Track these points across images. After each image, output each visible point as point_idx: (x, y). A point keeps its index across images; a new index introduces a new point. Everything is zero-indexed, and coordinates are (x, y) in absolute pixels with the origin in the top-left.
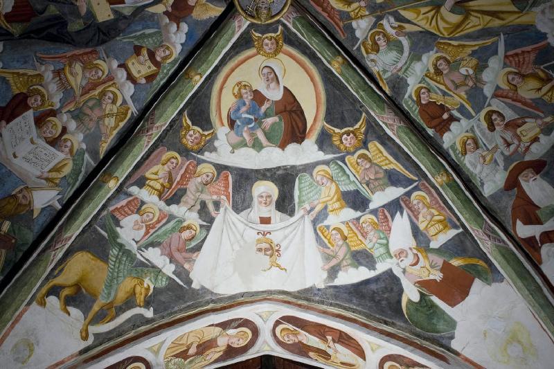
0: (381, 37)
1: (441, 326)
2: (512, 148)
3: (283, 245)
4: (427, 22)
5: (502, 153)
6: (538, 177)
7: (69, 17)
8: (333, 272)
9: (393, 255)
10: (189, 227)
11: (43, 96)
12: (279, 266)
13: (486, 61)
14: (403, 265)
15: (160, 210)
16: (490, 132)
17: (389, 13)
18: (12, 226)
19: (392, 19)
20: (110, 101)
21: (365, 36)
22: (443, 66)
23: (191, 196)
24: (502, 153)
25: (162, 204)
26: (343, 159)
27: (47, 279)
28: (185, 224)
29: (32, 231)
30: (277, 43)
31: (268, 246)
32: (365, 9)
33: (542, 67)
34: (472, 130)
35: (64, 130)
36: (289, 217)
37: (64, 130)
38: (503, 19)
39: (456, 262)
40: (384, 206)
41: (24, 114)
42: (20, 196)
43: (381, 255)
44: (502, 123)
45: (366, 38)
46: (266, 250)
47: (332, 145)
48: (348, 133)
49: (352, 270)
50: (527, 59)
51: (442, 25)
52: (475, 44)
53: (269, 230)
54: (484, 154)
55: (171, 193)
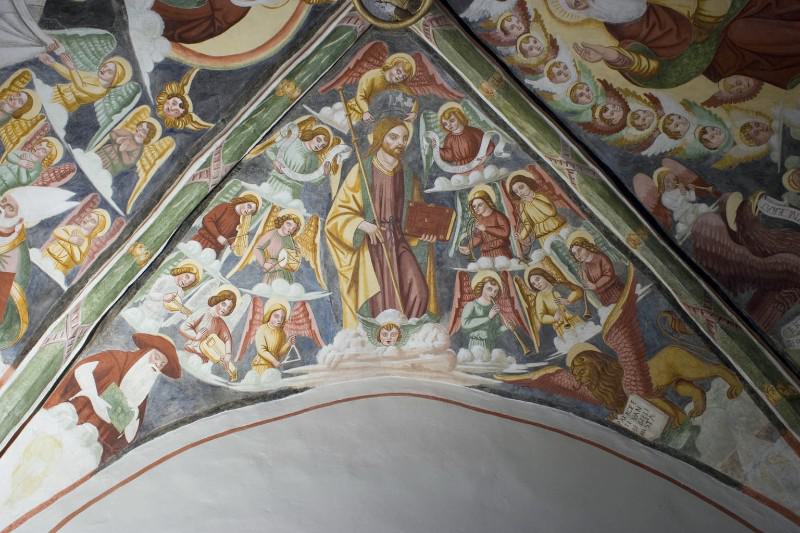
0: (323, 142)
2: (191, 333)
4: (343, 202)
6: (159, 372)
13: (298, 281)
19: (346, 156)
24: (181, 322)
26: (143, 101)
33: (293, 346)
34: (208, 277)
36: (38, 19)
38: (349, 292)
39: (16, 292)
40: (80, 170)
45: (320, 122)
47: (164, 82)
48: (184, 105)
50: (302, 327)
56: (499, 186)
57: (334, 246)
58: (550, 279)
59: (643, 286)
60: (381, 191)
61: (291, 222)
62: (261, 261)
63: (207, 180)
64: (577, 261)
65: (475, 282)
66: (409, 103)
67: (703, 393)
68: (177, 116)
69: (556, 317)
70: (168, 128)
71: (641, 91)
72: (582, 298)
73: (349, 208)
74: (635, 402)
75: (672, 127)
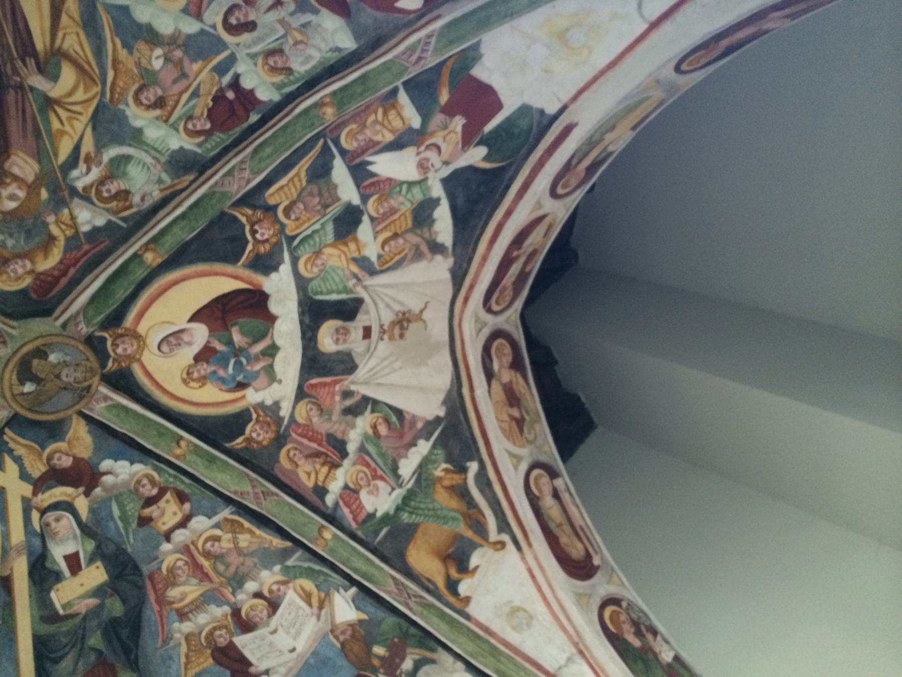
0: (104, 189)
1: (524, 124)
3: (397, 308)
5: (292, 14)
7: (104, 617)
8: (436, 248)
9: (423, 177)
10: (374, 427)
11: (215, 629)
12: (421, 311)
13: (139, 26)
14: (438, 164)
15: (354, 464)
16: (258, 29)
17: (64, 179)
18: (378, 643)
19: (75, 173)
20: (217, 544)
21: (105, 212)
22: (149, 96)
23: (336, 427)
24: (292, 14)
25: (346, 463)
26: (291, 239)
27: (439, 597)
28: (370, 432)
29: (384, 619)
30: (121, 336)
32: (60, 215)
34: (253, 56)
35: (258, 595)
36: (364, 305)
37: (258, 595)
39: (444, 97)
40: (358, 186)
41: (240, 647)
42: (342, 638)
43: (423, 192)
44: (243, 9)
45: (108, 210)
46: (402, 328)
48: (254, 232)
49: (437, 227)
51: (80, 95)
52: (112, 43)
54: (291, 41)
55: (333, 453)
57: (89, 63)
60: (24, 129)
61: (145, 101)
62: (186, 62)
68: (262, 223)
70: (271, 213)
73: (68, 110)
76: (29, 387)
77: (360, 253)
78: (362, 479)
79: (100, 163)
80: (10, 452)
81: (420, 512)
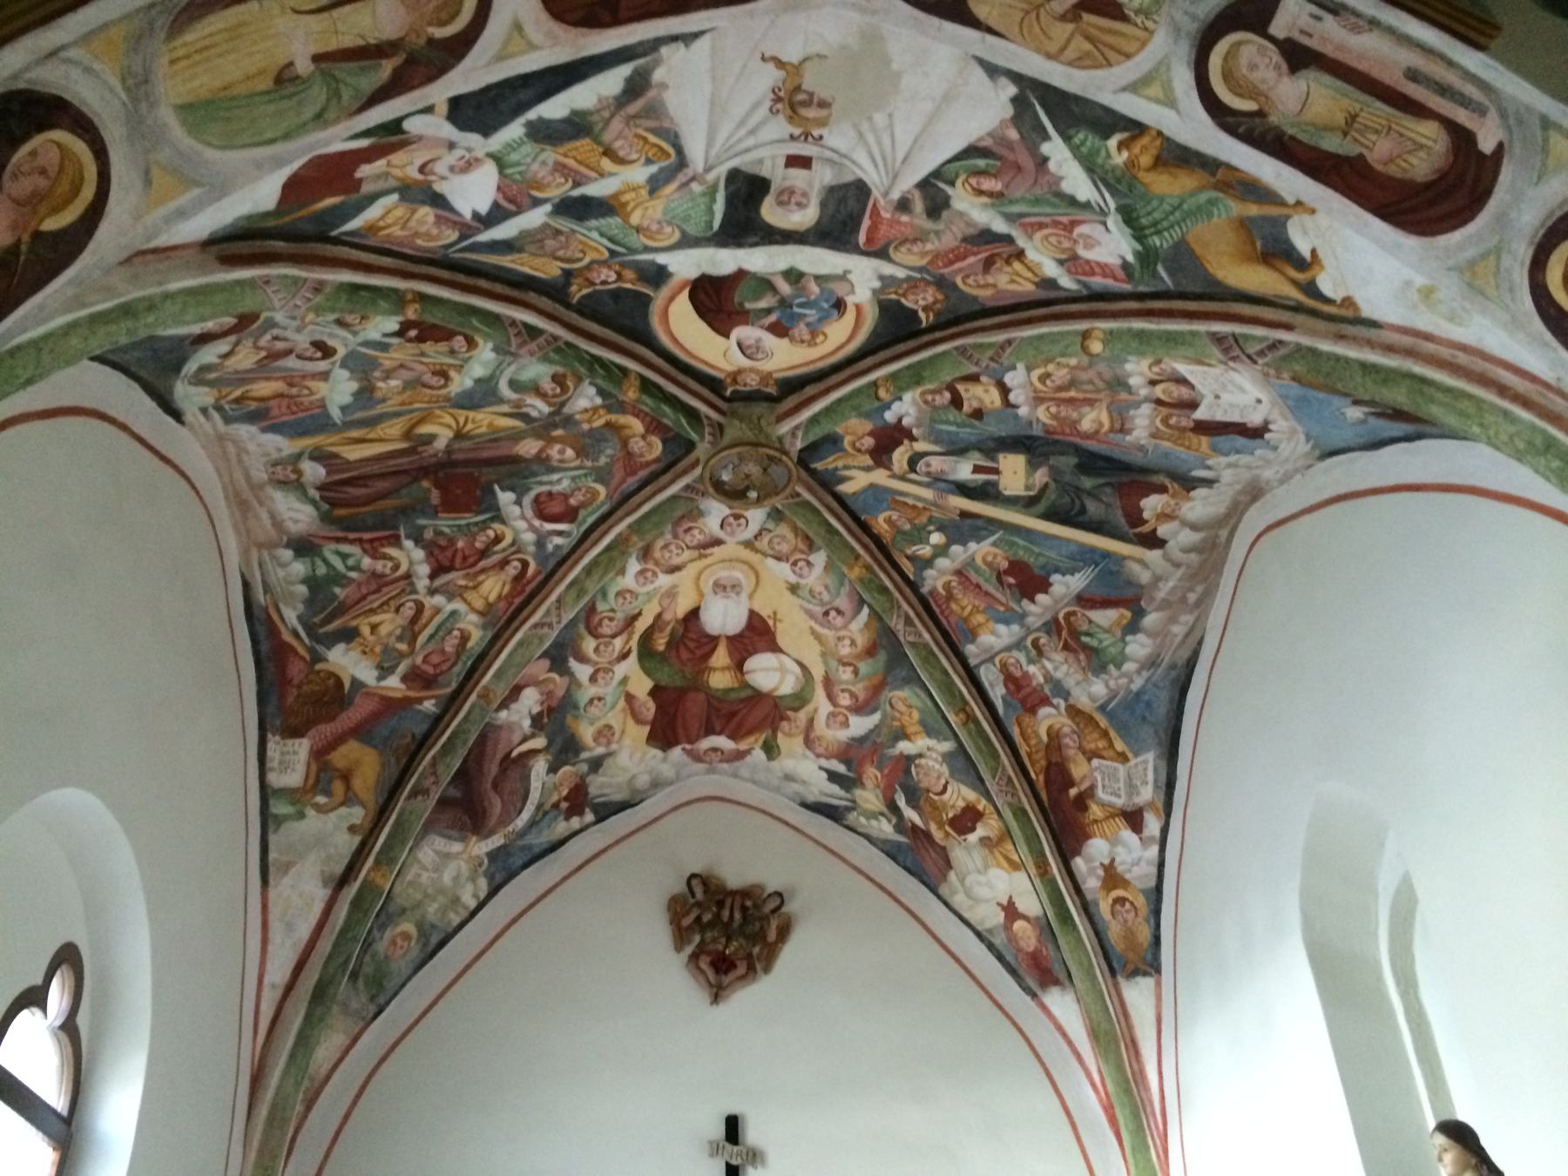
0: (550, 393)
3: (763, 111)
12: (780, 64)
19: (534, 414)
25: (1021, 242)
26: (613, 253)
31: (804, 112)
46: (807, 104)
53: (794, 144)
56: (513, 549)
58: (414, 620)
59: (434, 705)
63: (514, 346)
64: (443, 639)
65: (392, 552)
66: (603, 460)
67: (342, 804)
69: (371, 638)
71: (634, 643)
72: (402, 656)
74: (301, 749)
75: (601, 674)
76: (753, 495)
77: (639, 187)
78: (1060, 242)
79: (520, 400)
80: (836, 469)
81: (1165, 224)
